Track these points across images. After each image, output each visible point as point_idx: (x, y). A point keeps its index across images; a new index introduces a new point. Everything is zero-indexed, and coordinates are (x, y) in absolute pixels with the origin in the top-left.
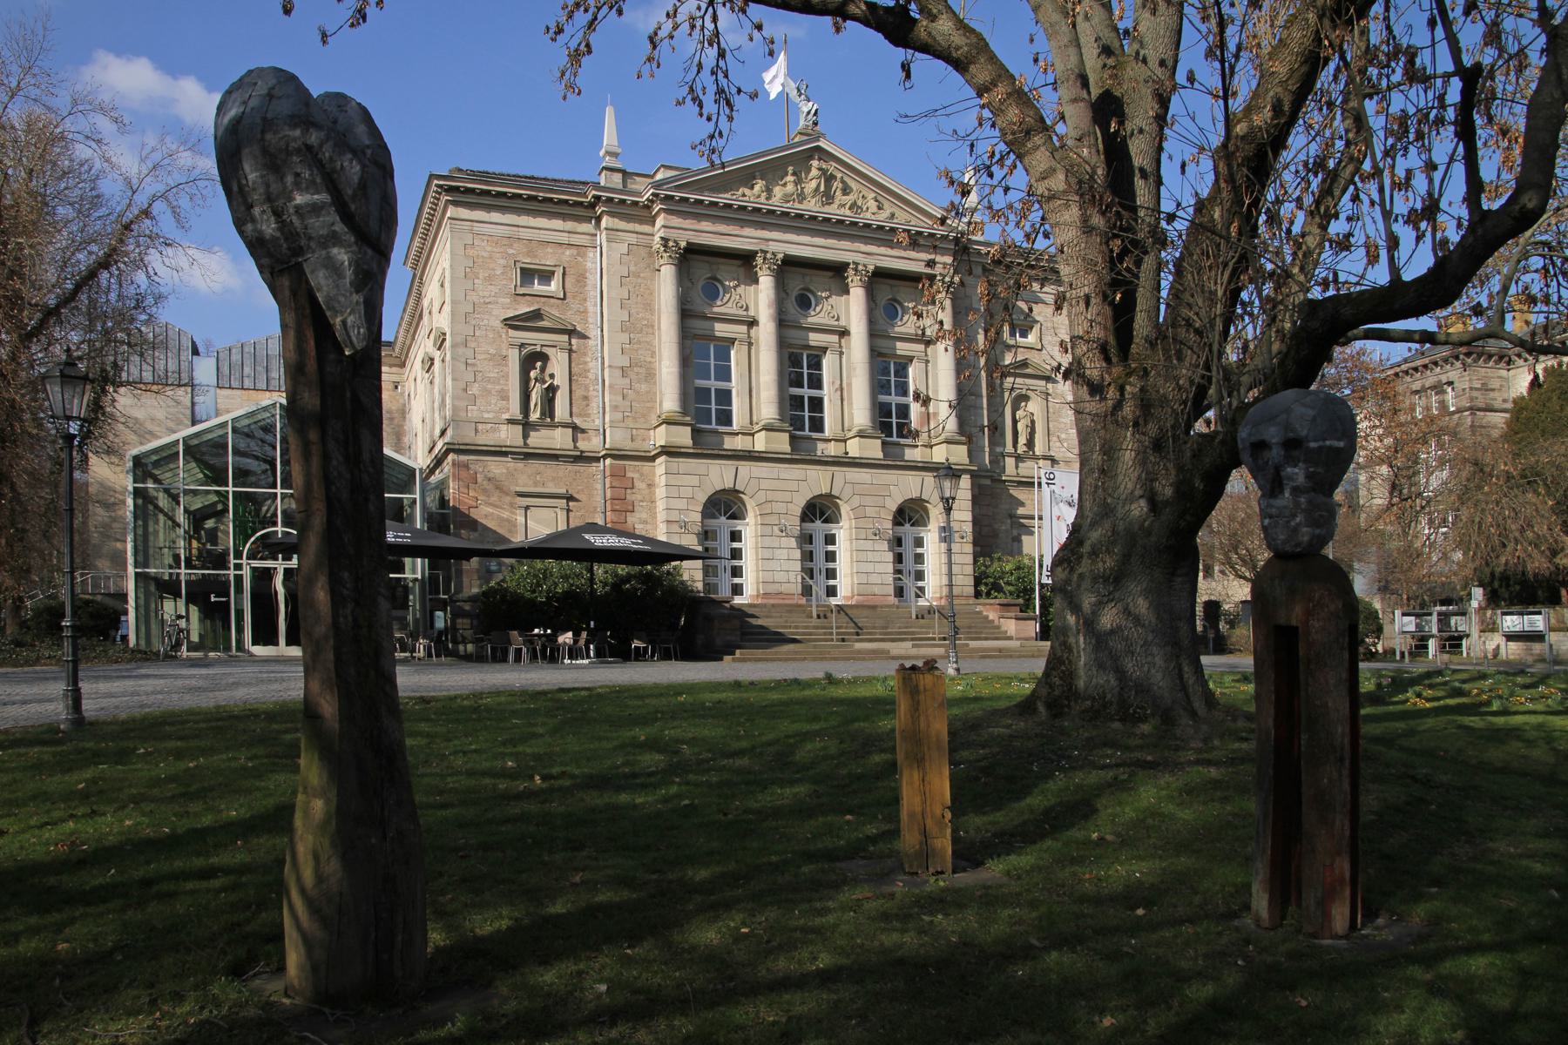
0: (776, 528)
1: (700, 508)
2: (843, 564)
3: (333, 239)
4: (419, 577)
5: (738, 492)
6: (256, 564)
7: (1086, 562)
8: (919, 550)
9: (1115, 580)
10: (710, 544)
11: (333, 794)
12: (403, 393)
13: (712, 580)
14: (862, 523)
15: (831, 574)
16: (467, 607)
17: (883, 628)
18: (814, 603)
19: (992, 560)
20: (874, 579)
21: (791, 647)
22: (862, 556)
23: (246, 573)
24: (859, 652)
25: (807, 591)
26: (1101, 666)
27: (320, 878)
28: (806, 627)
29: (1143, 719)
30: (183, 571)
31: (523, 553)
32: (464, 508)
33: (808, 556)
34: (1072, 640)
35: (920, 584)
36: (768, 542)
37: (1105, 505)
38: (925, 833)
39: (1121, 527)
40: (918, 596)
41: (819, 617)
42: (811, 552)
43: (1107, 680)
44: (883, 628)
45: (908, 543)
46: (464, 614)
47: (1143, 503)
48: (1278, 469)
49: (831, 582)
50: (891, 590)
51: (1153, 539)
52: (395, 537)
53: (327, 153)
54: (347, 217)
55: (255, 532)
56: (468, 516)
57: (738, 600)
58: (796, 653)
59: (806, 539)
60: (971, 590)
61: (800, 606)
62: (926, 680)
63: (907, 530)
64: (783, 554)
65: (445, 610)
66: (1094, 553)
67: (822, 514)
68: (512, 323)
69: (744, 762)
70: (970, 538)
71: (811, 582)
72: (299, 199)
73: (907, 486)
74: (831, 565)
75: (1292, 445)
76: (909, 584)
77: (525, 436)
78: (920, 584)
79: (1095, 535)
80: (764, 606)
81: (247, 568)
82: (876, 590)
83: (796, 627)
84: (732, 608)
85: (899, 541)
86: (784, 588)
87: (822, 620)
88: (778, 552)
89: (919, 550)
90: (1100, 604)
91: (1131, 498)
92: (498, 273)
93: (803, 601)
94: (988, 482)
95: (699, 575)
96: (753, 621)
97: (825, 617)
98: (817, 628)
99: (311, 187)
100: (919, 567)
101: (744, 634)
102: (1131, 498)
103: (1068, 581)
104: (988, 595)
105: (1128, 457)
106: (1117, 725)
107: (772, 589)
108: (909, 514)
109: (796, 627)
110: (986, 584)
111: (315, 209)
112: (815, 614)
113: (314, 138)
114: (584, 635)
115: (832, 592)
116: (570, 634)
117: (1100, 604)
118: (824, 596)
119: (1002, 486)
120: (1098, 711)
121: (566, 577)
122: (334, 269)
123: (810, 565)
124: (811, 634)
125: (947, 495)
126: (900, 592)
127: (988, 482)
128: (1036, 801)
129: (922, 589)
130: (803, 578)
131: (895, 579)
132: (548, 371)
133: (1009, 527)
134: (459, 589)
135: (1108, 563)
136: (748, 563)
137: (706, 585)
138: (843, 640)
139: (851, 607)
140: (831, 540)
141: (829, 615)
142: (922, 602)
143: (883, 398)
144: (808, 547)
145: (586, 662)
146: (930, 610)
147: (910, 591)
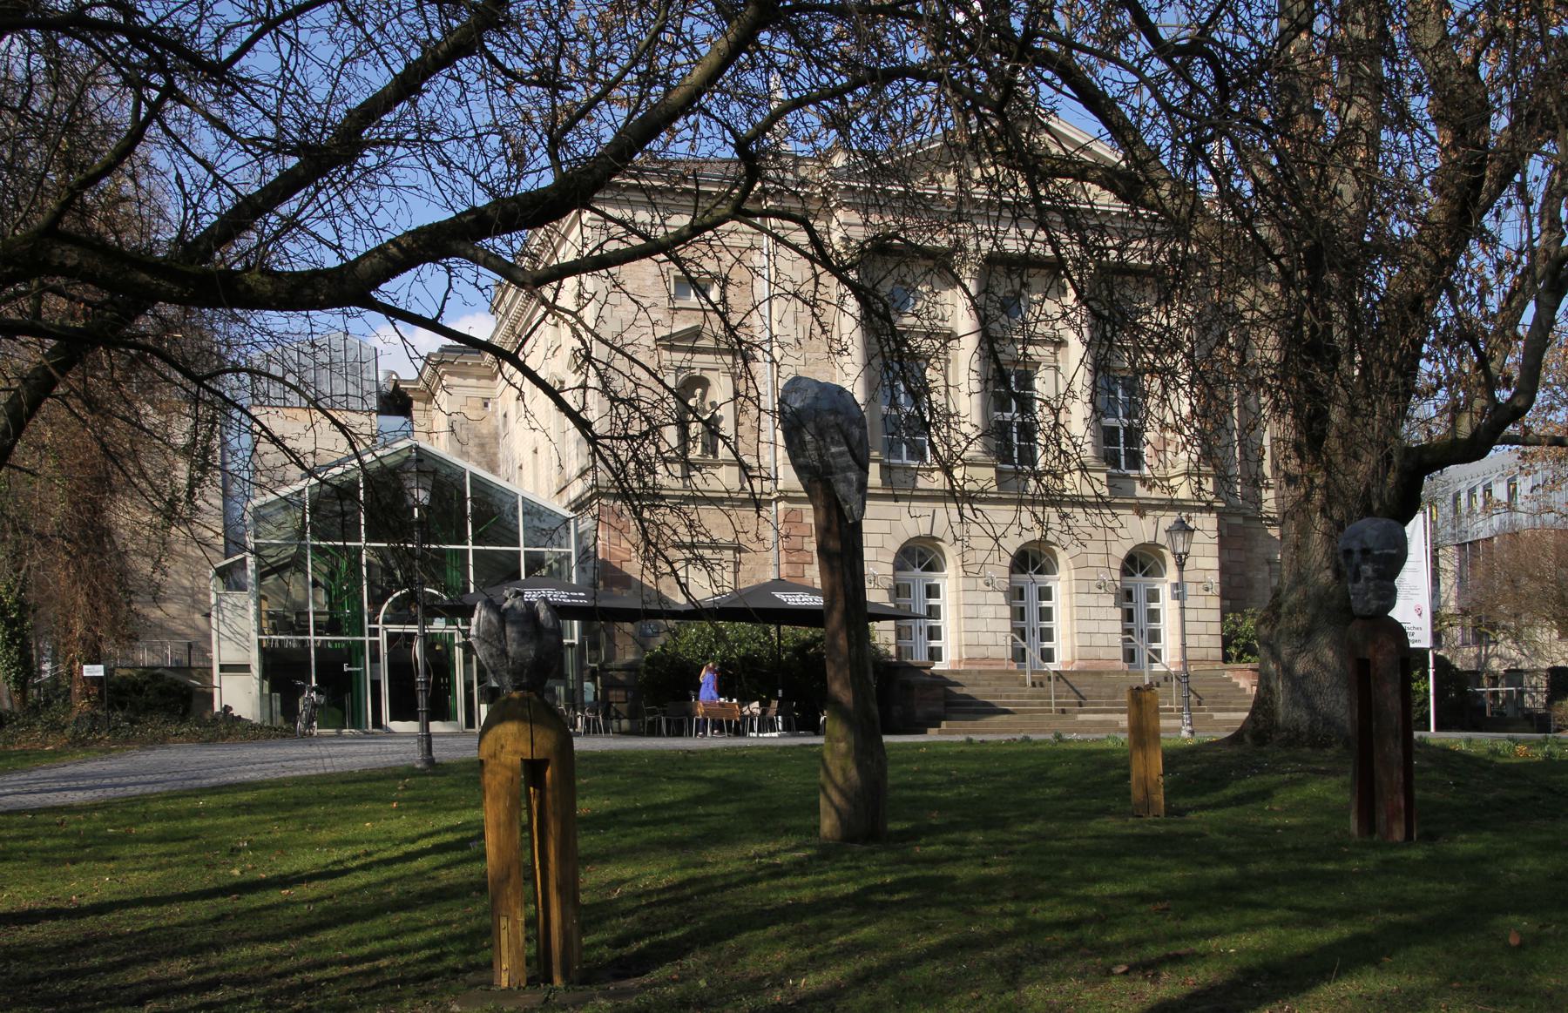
0: (980, 581)
1: (891, 559)
2: (1061, 623)
3: (849, 468)
4: (576, 641)
5: (935, 539)
6: (395, 628)
7: (1283, 620)
8: (1153, 606)
9: (1307, 635)
10: (903, 601)
11: (852, 739)
12: (494, 413)
13: (905, 643)
14: (1084, 574)
15: (1047, 635)
16: (621, 677)
17: (1109, 697)
18: (1028, 670)
19: (1244, 616)
20: (1100, 640)
21: (1005, 717)
22: (1085, 614)
23: (382, 638)
24: (1083, 722)
25: (1019, 655)
26: (1296, 704)
27: (846, 779)
28: (1021, 697)
29: (1328, 745)
30: (312, 637)
31: (696, 613)
32: (615, 562)
33: (1018, 614)
34: (1273, 684)
35: (1155, 646)
36: (971, 597)
37: (1299, 574)
38: (1146, 791)
39: (1311, 591)
40: (1152, 660)
41: (1034, 685)
42: (1022, 609)
43: (1301, 716)
44: (1109, 697)
45: (1140, 595)
46: (619, 686)
47: (1329, 573)
48: (1358, 566)
49: (1047, 645)
50: (1119, 654)
51: (1335, 602)
52: (570, 597)
53: (845, 426)
54: (854, 456)
55: (391, 594)
56: (621, 571)
57: (938, 667)
58: (1010, 724)
59: (1016, 593)
60: (1218, 653)
61: (1012, 672)
62: (1148, 695)
63: (1139, 582)
64: (989, 611)
65: (594, 680)
66: (1290, 612)
67: (1035, 564)
68: (669, 343)
69: (1009, 778)
70: (1216, 590)
71: (1024, 645)
72: (833, 450)
73: (1137, 530)
74: (1046, 624)
75: (1365, 552)
76: (1142, 647)
77: (686, 476)
78: (1155, 646)
79: (1293, 598)
80: (970, 672)
81: (384, 631)
82: (1102, 654)
83: (1008, 697)
84: (933, 675)
85: (1129, 595)
86: (992, 652)
87: (1038, 689)
88: (983, 609)
89: (1153, 606)
90: (1294, 655)
91: (1320, 569)
92: (649, 283)
93: (1014, 667)
94: (1240, 521)
95: (892, 638)
96: (958, 690)
97: (1042, 685)
98: (1032, 697)
99: (838, 444)
100: (1154, 625)
101: (947, 705)
102: (1320, 569)
103: (1270, 637)
104: (1239, 658)
105: (1317, 537)
106: (1307, 750)
107: (977, 652)
108: (1141, 562)
109: (1008, 697)
110: (1237, 646)
111: (841, 454)
112: (1029, 682)
113: (840, 419)
114: (775, 704)
115: (1047, 655)
116: (756, 704)
117: (1294, 655)
118: (1038, 659)
119: (1257, 524)
120: (1293, 739)
121: (741, 641)
122: (848, 481)
123: (1020, 624)
124: (1025, 704)
125: (1180, 550)
126: (1130, 656)
127: (1240, 521)
128: (1229, 792)
129: (1157, 652)
130: (1014, 640)
131: (1124, 640)
132: (709, 399)
133: (1266, 575)
134: (611, 656)
135: (1301, 621)
136: (948, 622)
137: (898, 649)
138: (1063, 711)
139: (1071, 673)
140: (1045, 594)
141: (1046, 682)
142: (1157, 668)
143: (1110, 422)
144: (1019, 604)
145: (775, 734)
146: (1167, 677)
147: (1143, 655)
